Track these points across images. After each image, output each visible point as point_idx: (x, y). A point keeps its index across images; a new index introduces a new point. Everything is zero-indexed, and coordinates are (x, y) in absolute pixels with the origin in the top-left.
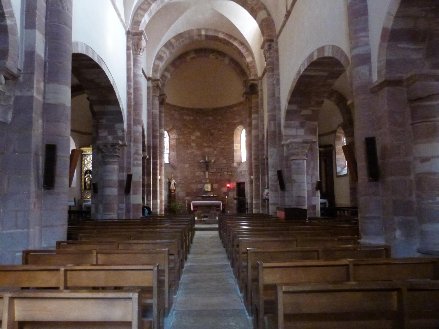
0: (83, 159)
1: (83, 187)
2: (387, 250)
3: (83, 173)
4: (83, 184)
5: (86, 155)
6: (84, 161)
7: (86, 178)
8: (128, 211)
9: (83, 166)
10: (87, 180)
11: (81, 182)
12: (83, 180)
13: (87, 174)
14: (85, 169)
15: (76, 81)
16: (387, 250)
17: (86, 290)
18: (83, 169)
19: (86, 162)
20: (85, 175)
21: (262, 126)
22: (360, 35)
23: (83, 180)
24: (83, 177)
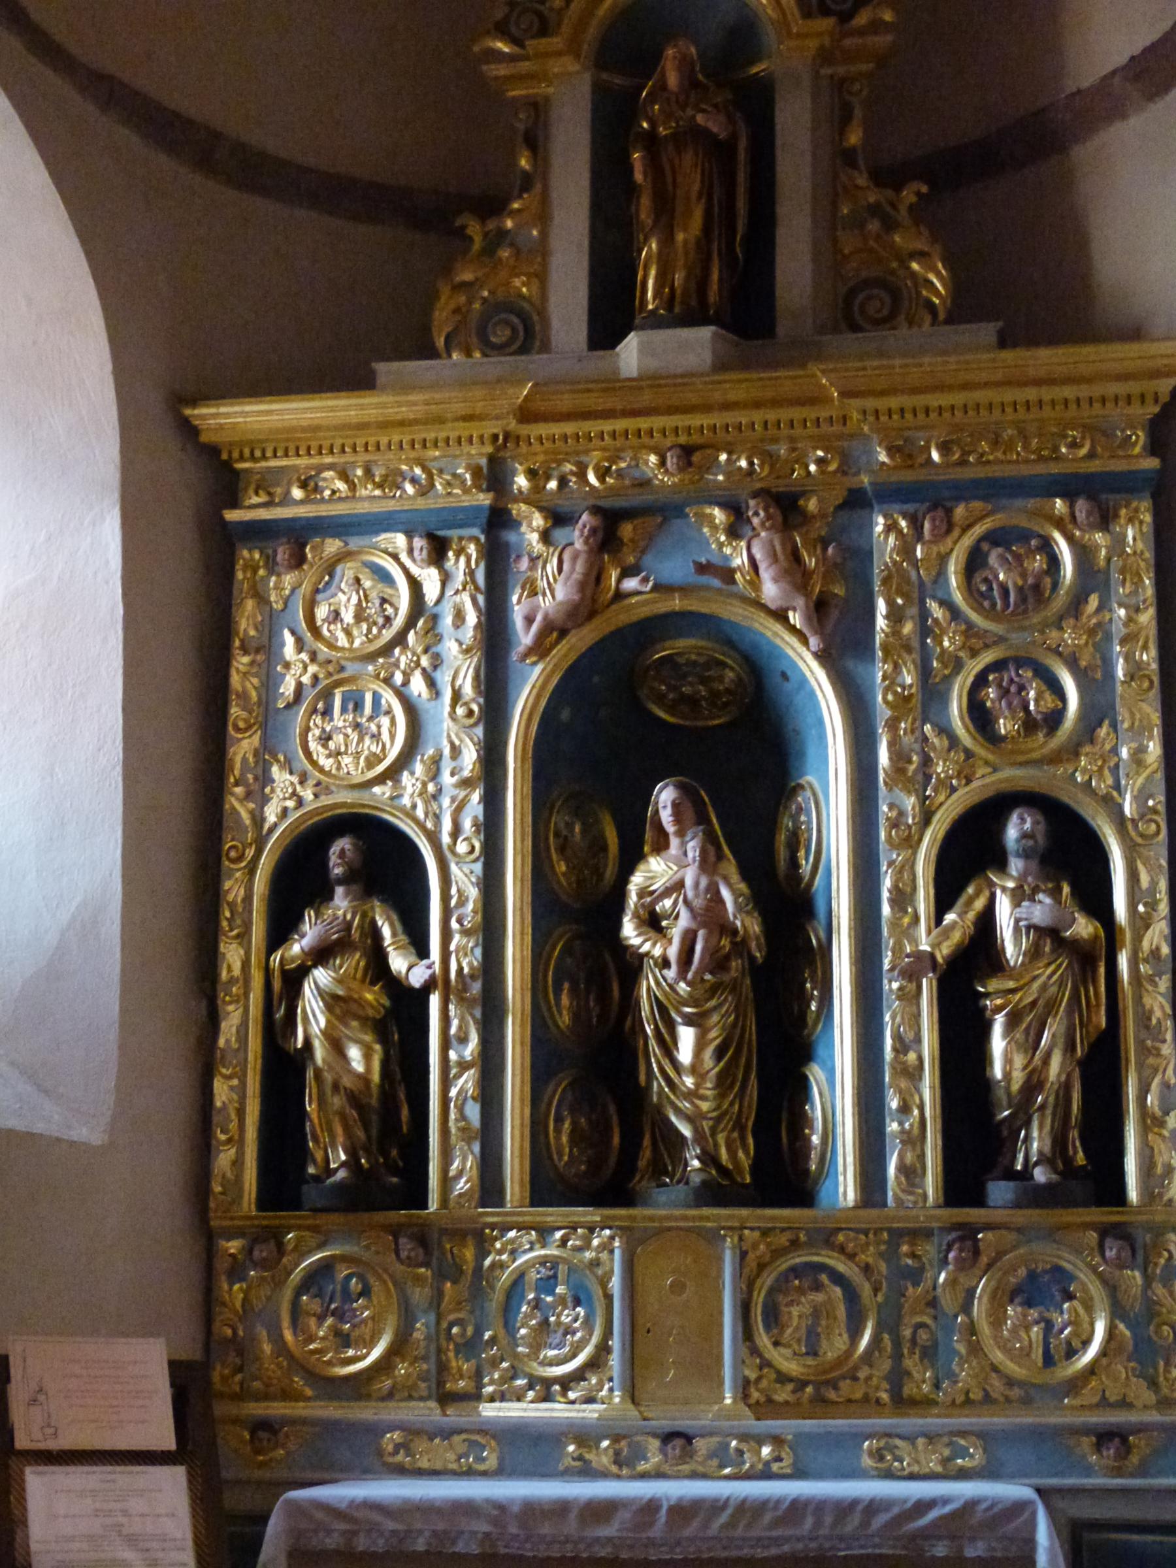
0: (246, 620)
1: (239, 1160)
2: (1092, 741)
3: (250, 887)
4: (239, 1094)
5: (297, 538)
6: (268, 649)
7: (294, 979)
8: (451, 1445)
9: (243, 748)
10: (313, 1014)
11: (206, 1061)
12: (240, 1023)
13: (321, 894)
14: (283, 803)
15: (516, 1509)
16: (1092, 741)
17: (345, 520)
18: (237, 804)
19: (296, 669)
20: (282, 928)
21: (1145, 880)
22: (1066, 1255)
23: (240, 1023)
24: (232, 955)
